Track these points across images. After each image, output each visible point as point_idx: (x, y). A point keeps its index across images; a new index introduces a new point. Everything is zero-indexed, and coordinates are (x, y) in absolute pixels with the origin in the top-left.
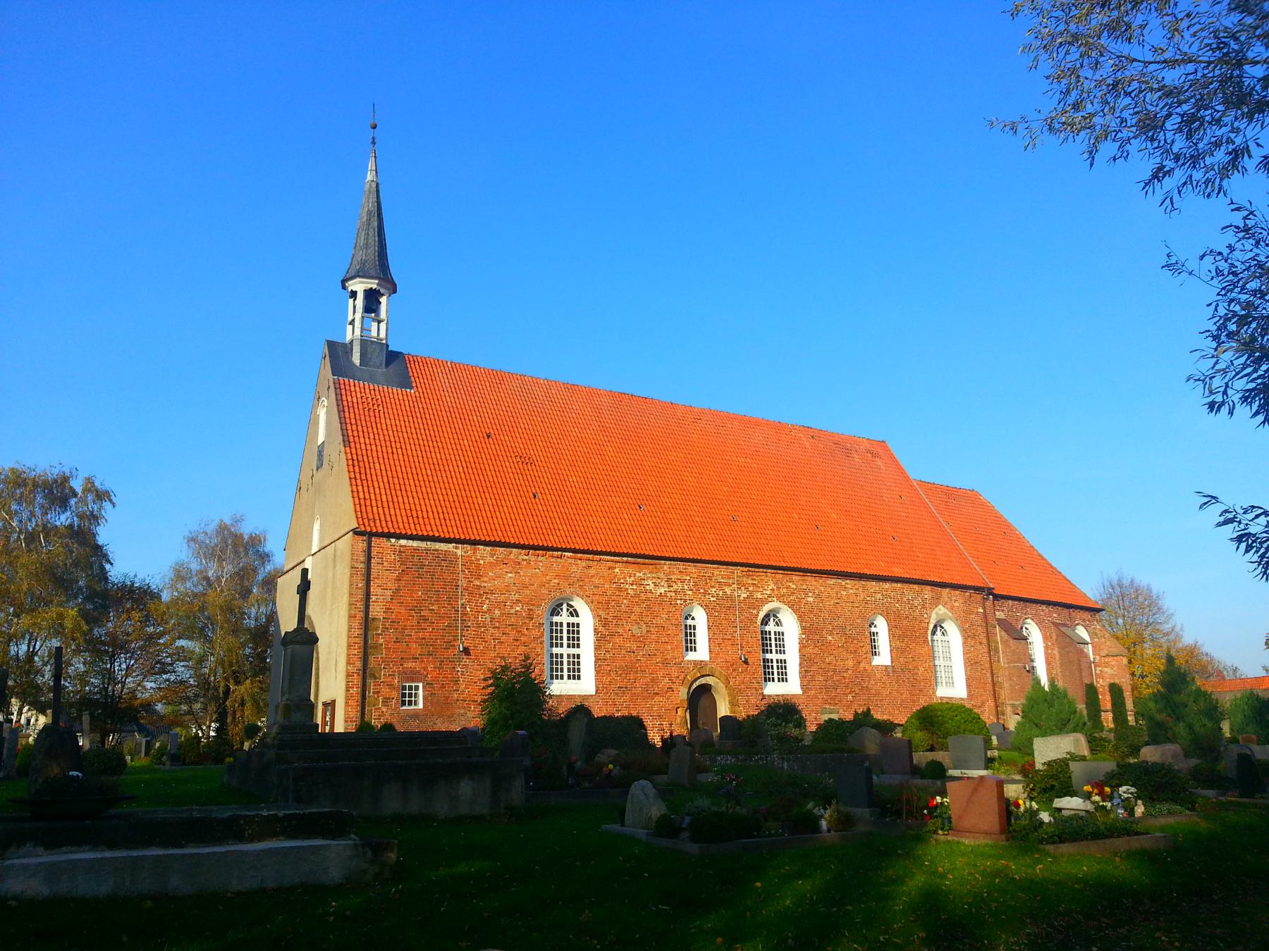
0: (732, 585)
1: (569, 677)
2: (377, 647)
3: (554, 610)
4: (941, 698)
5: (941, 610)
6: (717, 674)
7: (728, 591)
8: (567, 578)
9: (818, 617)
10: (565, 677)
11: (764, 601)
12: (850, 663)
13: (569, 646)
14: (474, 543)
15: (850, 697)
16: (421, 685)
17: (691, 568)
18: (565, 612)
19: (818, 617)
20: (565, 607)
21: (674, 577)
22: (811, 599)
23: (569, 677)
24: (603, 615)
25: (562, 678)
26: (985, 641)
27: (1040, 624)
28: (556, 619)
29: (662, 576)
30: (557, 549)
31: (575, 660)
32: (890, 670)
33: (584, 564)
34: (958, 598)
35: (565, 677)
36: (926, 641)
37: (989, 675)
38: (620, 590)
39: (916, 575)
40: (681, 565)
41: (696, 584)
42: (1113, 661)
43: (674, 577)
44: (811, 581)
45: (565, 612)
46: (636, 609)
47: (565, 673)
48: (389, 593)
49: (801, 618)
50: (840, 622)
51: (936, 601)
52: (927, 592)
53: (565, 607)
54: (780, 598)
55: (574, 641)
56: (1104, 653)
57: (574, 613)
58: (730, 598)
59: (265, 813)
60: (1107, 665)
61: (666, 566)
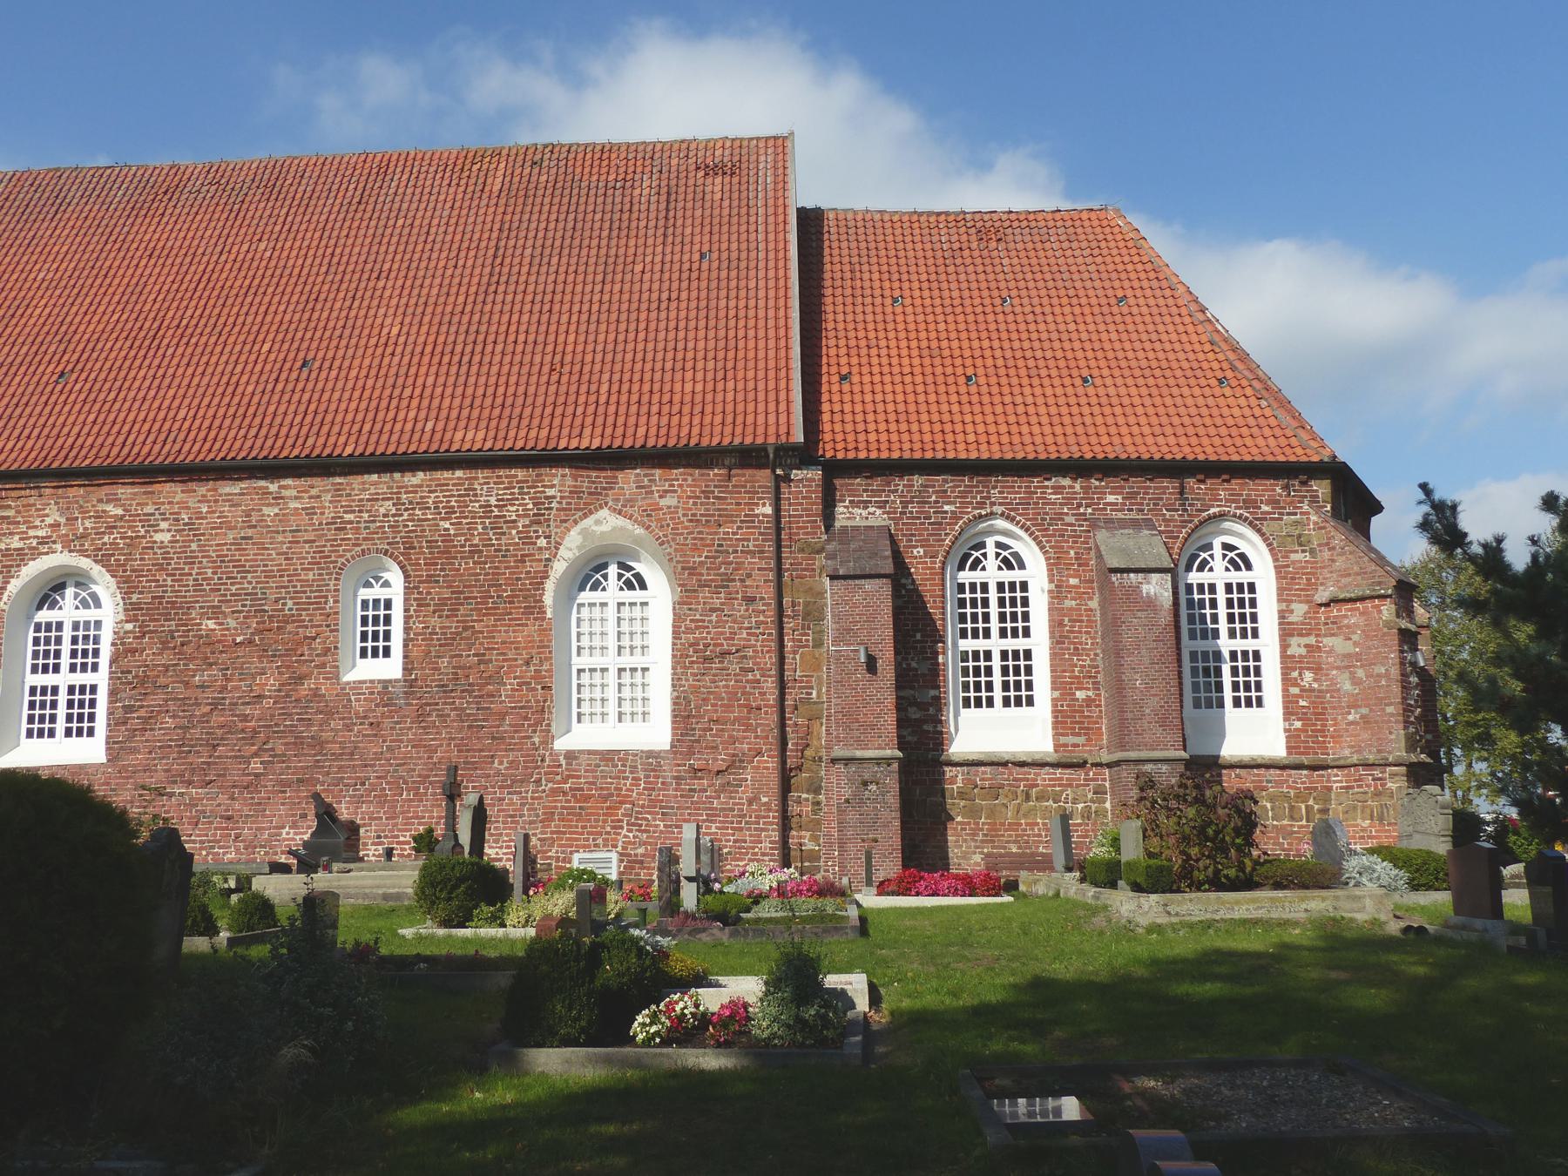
1: (1006, 702)
5: (605, 523)
10: (998, 701)
12: (270, 683)
13: (1003, 633)
15: (256, 765)
20: (613, 570)
23: (1006, 702)
25: (52, 734)
26: (768, 593)
27: (1040, 530)
31: (1019, 663)
34: (674, 491)
35: (998, 701)
37: (770, 684)
42: (1351, 616)
44: (173, 492)
52: (558, 482)
53: (613, 570)
55: (1015, 622)
56: (1322, 595)
57: (1011, 562)
60: (1335, 627)
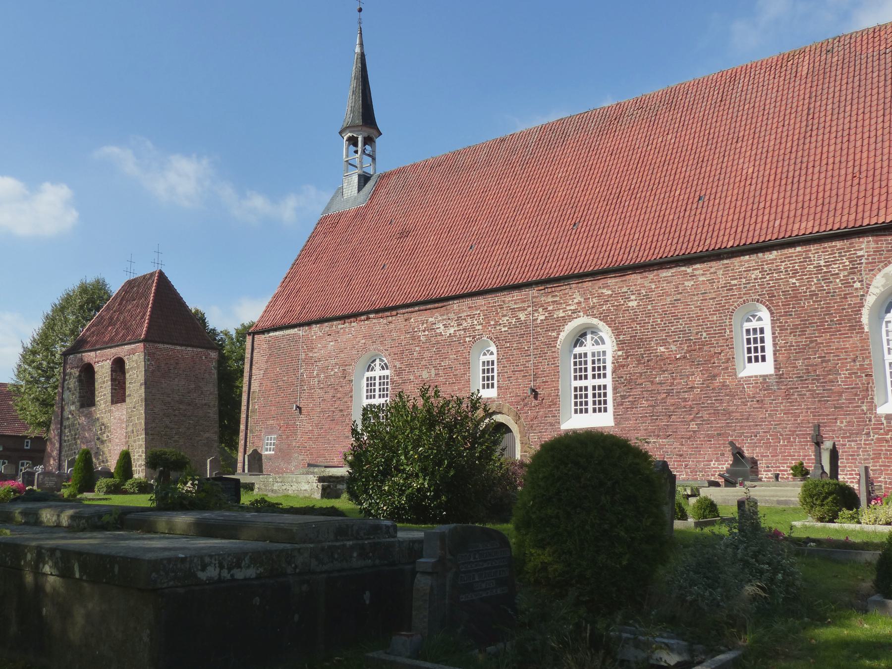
1: (594, 411)
2: (254, 411)
3: (578, 340)
4: (567, 432)
6: (505, 410)
7: (522, 316)
8: (371, 337)
9: (643, 324)
11: (565, 320)
12: (698, 380)
14: (309, 324)
17: (480, 301)
18: (378, 367)
19: (643, 324)
21: (463, 315)
22: (634, 304)
23: (594, 411)
24: (398, 365)
25: (586, 411)
28: (578, 350)
29: (452, 316)
30: (362, 314)
32: (773, 380)
33: (385, 321)
36: (857, 326)
38: (413, 338)
39: (837, 223)
40: (469, 302)
43: (463, 315)
44: (635, 278)
45: (378, 367)
47: (590, 407)
48: (262, 372)
49: (617, 331)
50: (681, 325)
54: (589, 311)
61: (455, 305)
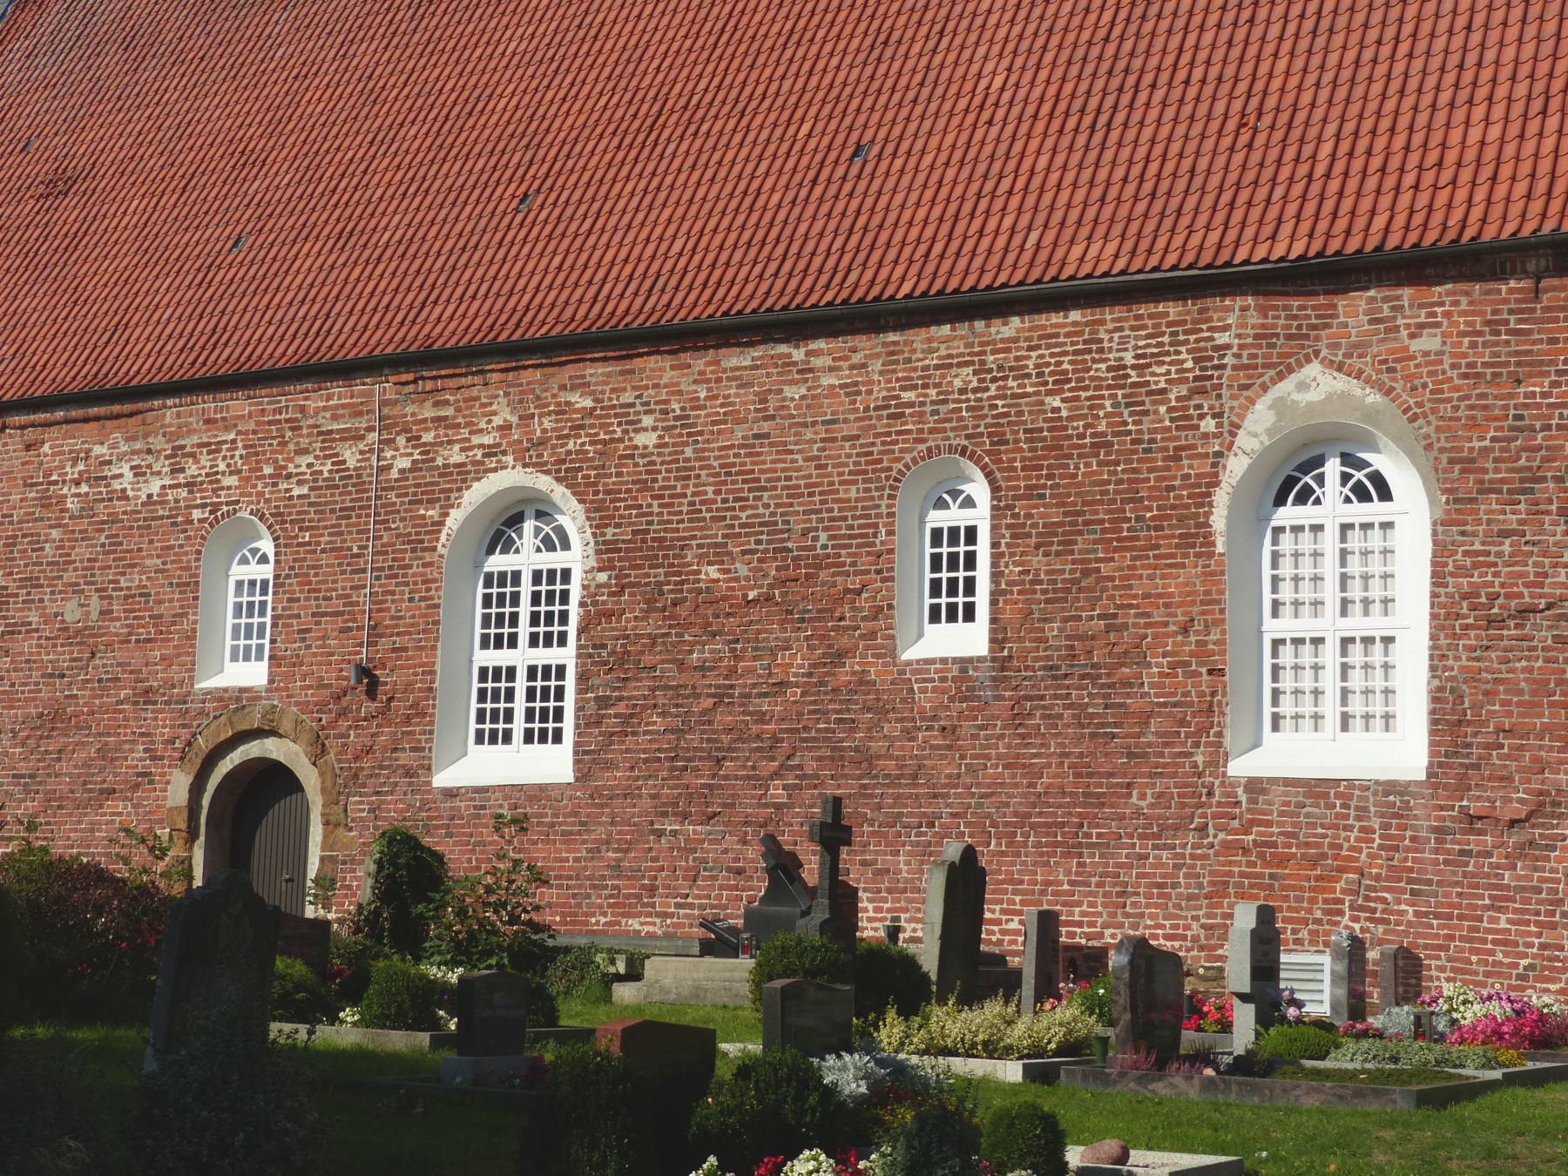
0: (339, 436)
1: (528, 737)
5: (1316, 387)
6: (286, 726)
7: (351, 457)
9: (668, 499)
11: (464, 475)
12: (797, 662)
16: (552, 764)
17: (238, 405)
20: (1332, 468)
21: (189, 442)
22: (647, 439)
23: (528, 737)
25: (507, 738)
28: (498, 562)
29: (157, 442)
32: (983, 674)
36: (1198, 537)
40: (207, 405)
41: (252, 453)
43: (189, 442)
44: (658, 368)
46: (81, 552)
47: (519, 726)
51: (1276, 358)
52: (1235, 321)
54: (530, 453)
58: (355, 480)
59: (40, 1031)
61: (170, 412)
